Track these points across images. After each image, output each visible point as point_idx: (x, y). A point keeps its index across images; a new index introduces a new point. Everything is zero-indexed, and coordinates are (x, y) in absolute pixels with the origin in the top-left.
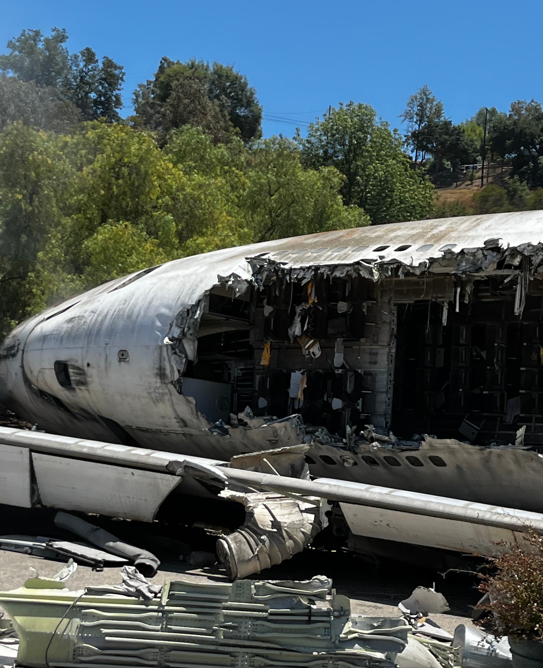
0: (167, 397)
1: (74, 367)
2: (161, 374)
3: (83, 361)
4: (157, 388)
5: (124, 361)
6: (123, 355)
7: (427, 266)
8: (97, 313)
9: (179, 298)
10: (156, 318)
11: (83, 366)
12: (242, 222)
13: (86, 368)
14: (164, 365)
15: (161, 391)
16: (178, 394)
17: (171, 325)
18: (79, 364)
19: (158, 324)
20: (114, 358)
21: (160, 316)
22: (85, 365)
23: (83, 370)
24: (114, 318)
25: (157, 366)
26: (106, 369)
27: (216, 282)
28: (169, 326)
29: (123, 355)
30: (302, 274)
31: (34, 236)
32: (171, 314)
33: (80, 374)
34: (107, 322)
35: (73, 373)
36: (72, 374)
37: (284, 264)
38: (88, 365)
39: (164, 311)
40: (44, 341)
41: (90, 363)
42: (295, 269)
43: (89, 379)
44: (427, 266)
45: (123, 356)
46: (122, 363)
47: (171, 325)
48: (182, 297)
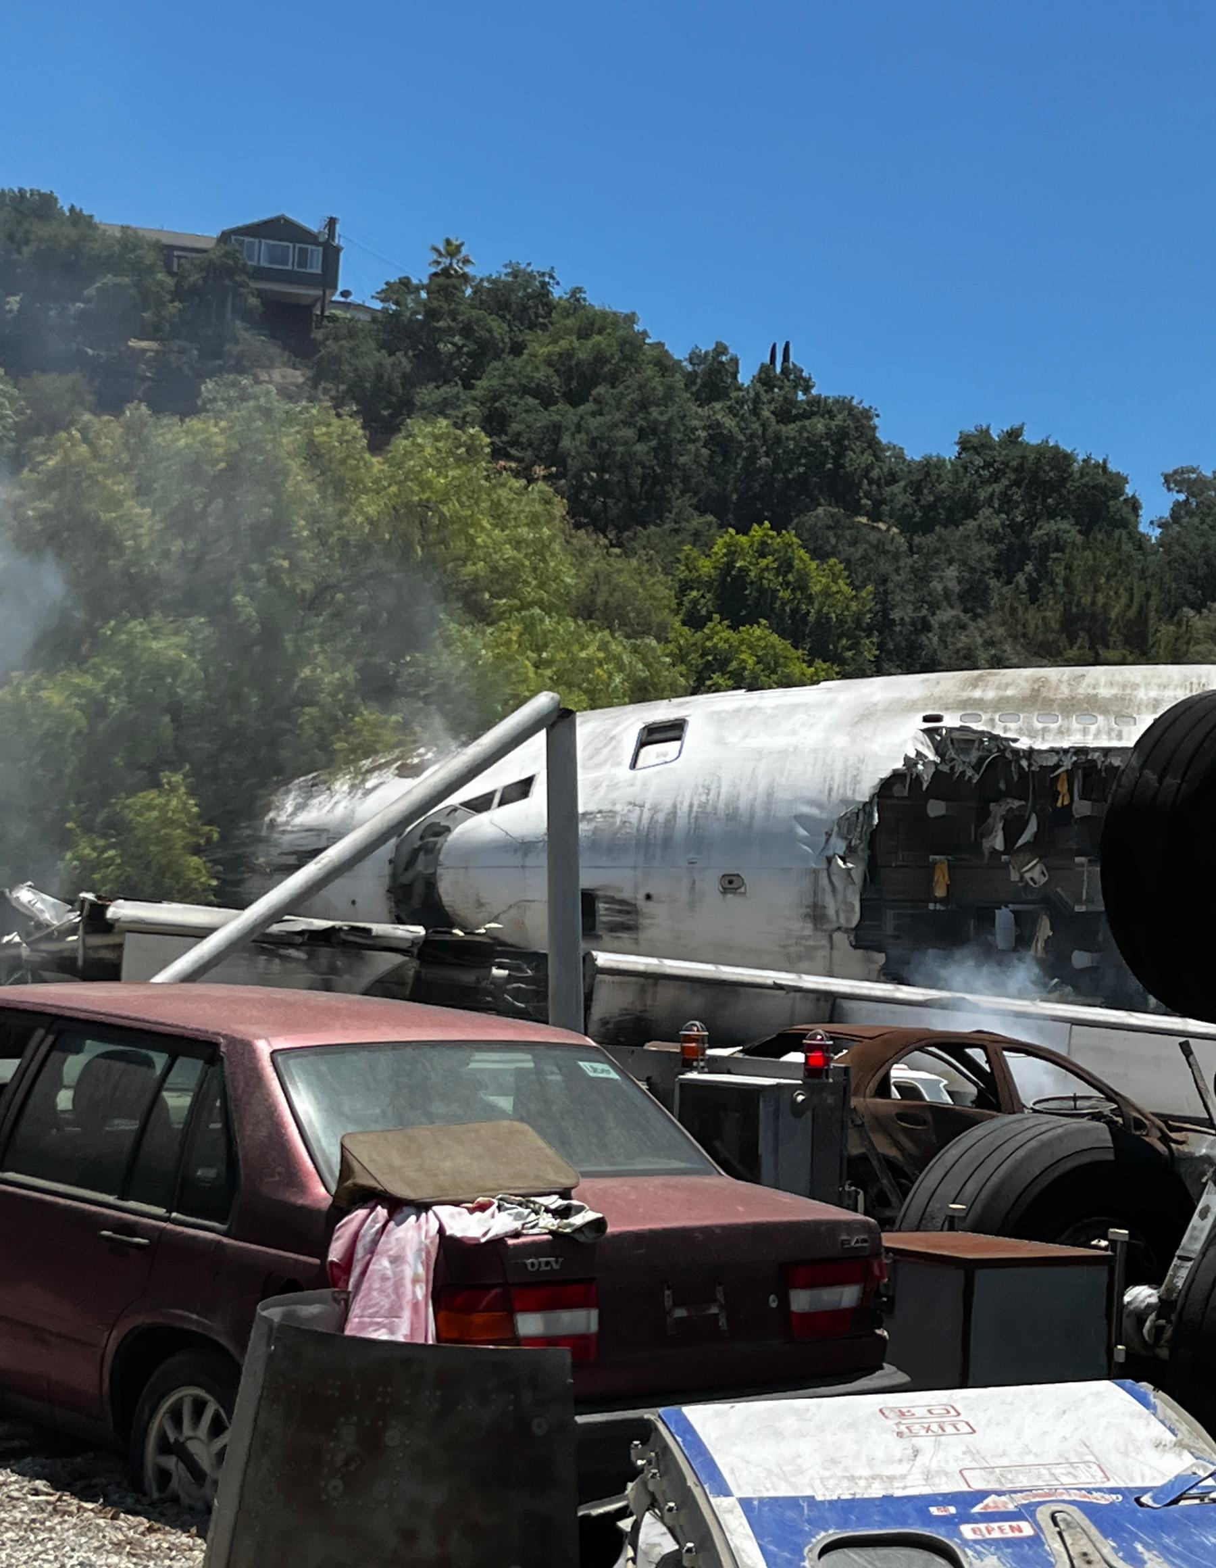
0: (821, 954)
1: (611, 900)
2: (816, 915)
3: (636, 887)
4: (804, 938)
5: (734, 893)
6: (730, 882)
7: (399, 763)
8: (647, 806)
9: (831, 790)
10: (794, 822)
11: (636, 899)
12: (523, 565)
13: (641, 903)
14: (823, 901)
15: (811, 943)
16: (851, 948)
17: (829, 835)
18: (626, 895)
19: (802, 832)
20: (710, 883)
21: (801, 819)
22: (641, 896)
23: (635, 905)
24: (696, 817)
25: (809, 901)
26: (692, 905)
27: (899, 765)
28: (824, 838)
29: (730, 882)
30: (1054, 760)
31: (529, 652)
32: (824, 816)
33: (628, 913)
34: (681, 822)
35: (607, 909)
36: (602, 912)
37: (1015, 740)
38: (648, 897)
39: (806, 809)
40: (525, 855)
41: (652, 892)
42: (1040, 752)
43: (644, 922)
44: (399, 763)
45: (731, 884)
46: (730, 896)
47: (829, 835)
48: (835, 787)
